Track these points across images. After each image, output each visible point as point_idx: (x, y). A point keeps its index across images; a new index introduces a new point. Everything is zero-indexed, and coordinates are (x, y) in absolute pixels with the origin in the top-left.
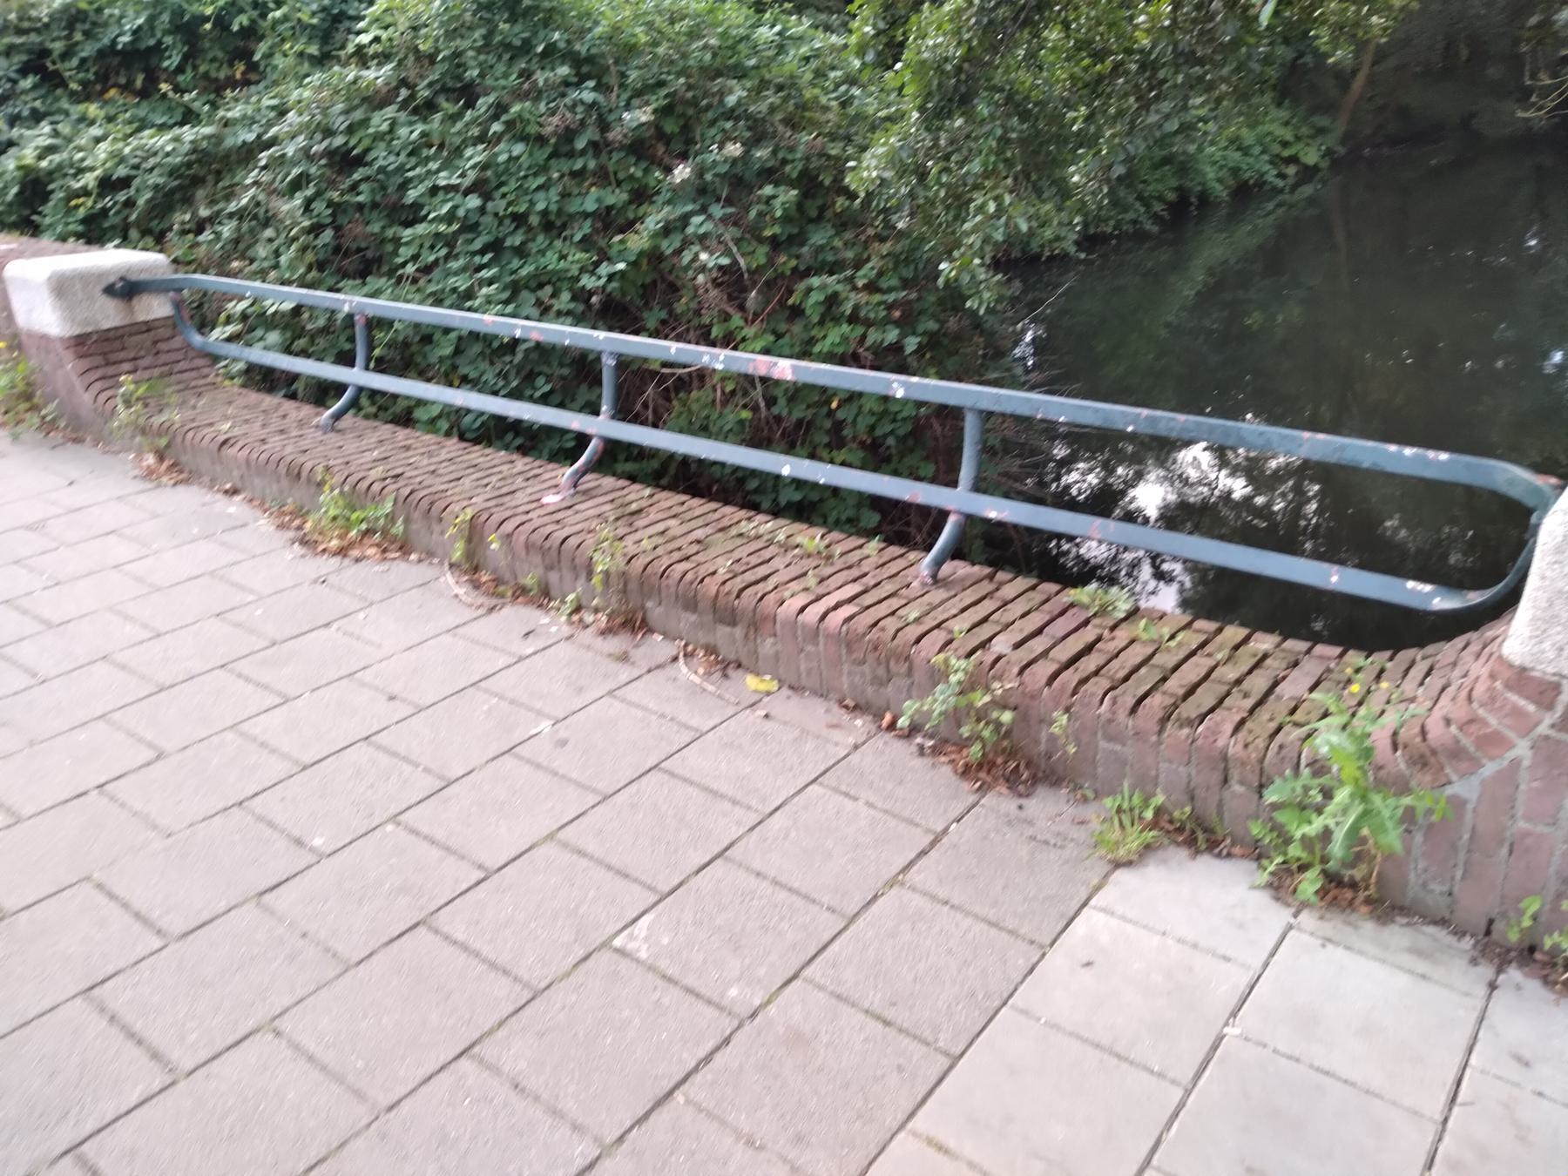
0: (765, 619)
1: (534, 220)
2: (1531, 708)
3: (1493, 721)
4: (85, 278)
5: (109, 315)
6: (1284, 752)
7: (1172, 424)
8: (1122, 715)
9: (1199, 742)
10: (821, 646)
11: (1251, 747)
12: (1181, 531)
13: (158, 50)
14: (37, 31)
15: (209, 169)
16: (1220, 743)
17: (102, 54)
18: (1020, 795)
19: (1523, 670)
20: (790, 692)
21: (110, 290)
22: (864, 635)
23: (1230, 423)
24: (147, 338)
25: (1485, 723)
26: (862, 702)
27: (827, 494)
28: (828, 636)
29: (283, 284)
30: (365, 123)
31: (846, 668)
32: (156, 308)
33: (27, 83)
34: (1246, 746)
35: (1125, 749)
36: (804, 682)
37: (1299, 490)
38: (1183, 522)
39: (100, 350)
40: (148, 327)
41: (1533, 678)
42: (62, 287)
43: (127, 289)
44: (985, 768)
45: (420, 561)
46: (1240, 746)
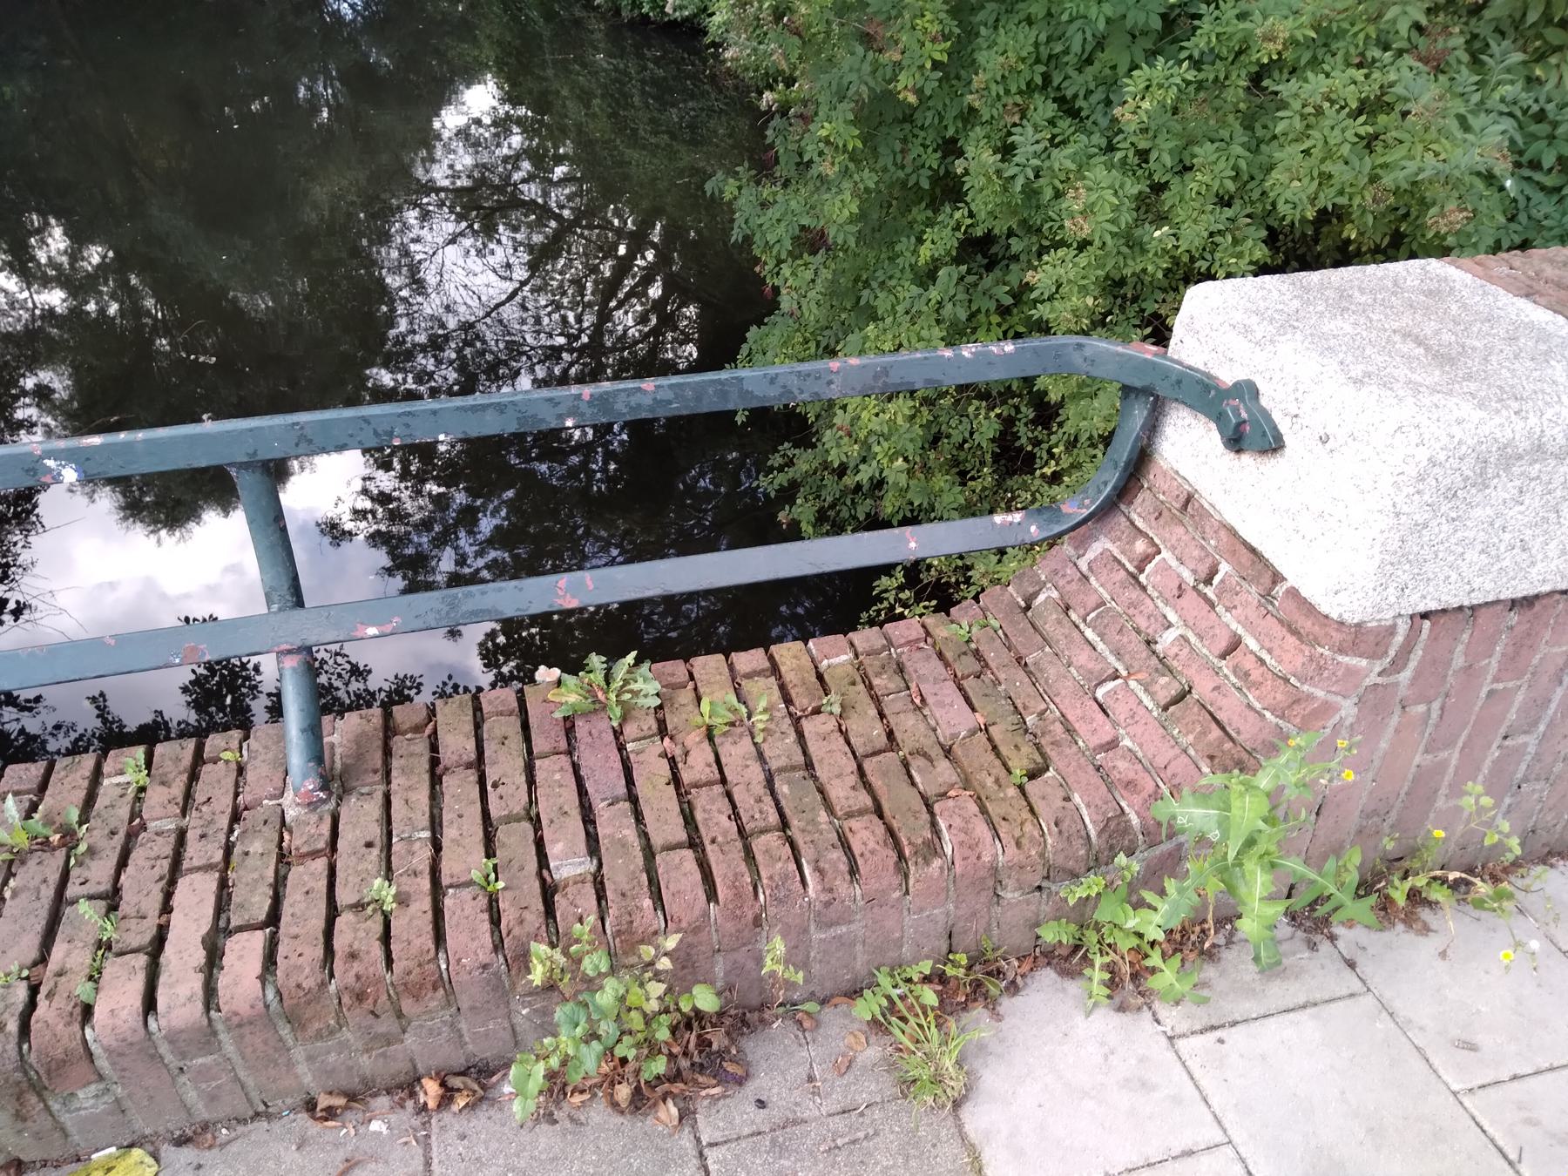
0: (58, 1067)
2: (1364, 662)
3: (1320, 694)
6: (1064, 826)
7: (634, 401)
8: (842, 887)
9: (958, 869)
10: (229, 1048)
11: (1024, 841)
12: (718, 550)
16: (986, 858)
18: (740, 1082)
19: (1358, 625)
20: (188, 1154)
22: (323, 985)
23: (723, 375)
25: (1310, 697)
26: (354, 1084)
28: (239, 1025)
31: (298, 1053)
34: (1018, 844)
35: (853, 927)
36: (203, 1113)
37: (124, 284)
38: (717, 538)
41: (1371, 630)
46: (1012, 850)
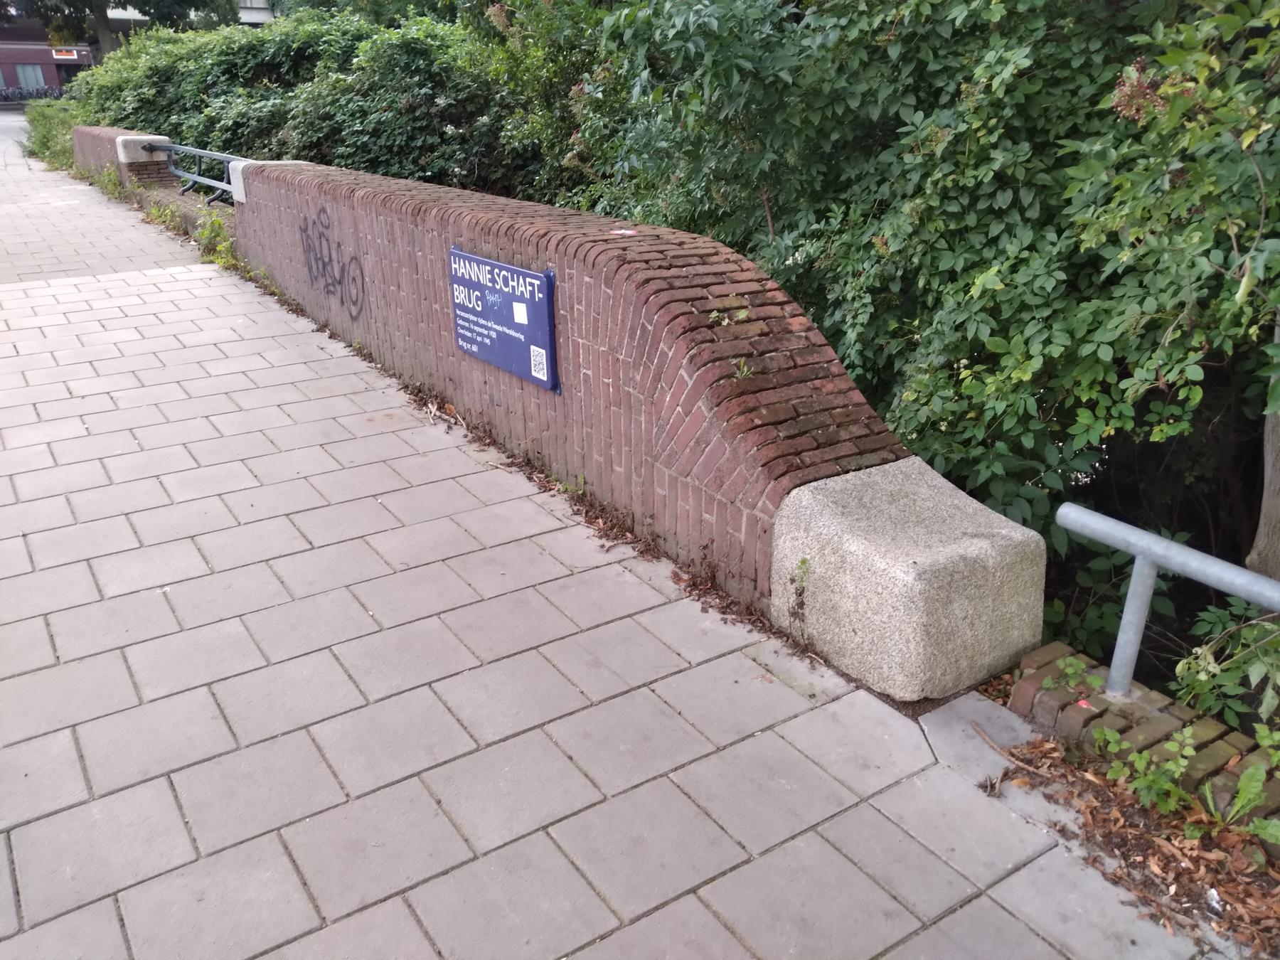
1: (395, 149)
4: (134, 142)
5: (143, 157)
13: (280, 65)
14: (234, 54)
15: (277, 120)
17: (258, 65)
21: (144, 148)
24: (156, 168)
27: (997, 490)
29: (90, 125)
30: (338, 100)
32: (162, 157)
33: (223, 78)
39: (136, 168)
40: (158, 163)
42: (126, 145)
43: (151, 148)
44: (190, 229)
45: (1116, 880)
